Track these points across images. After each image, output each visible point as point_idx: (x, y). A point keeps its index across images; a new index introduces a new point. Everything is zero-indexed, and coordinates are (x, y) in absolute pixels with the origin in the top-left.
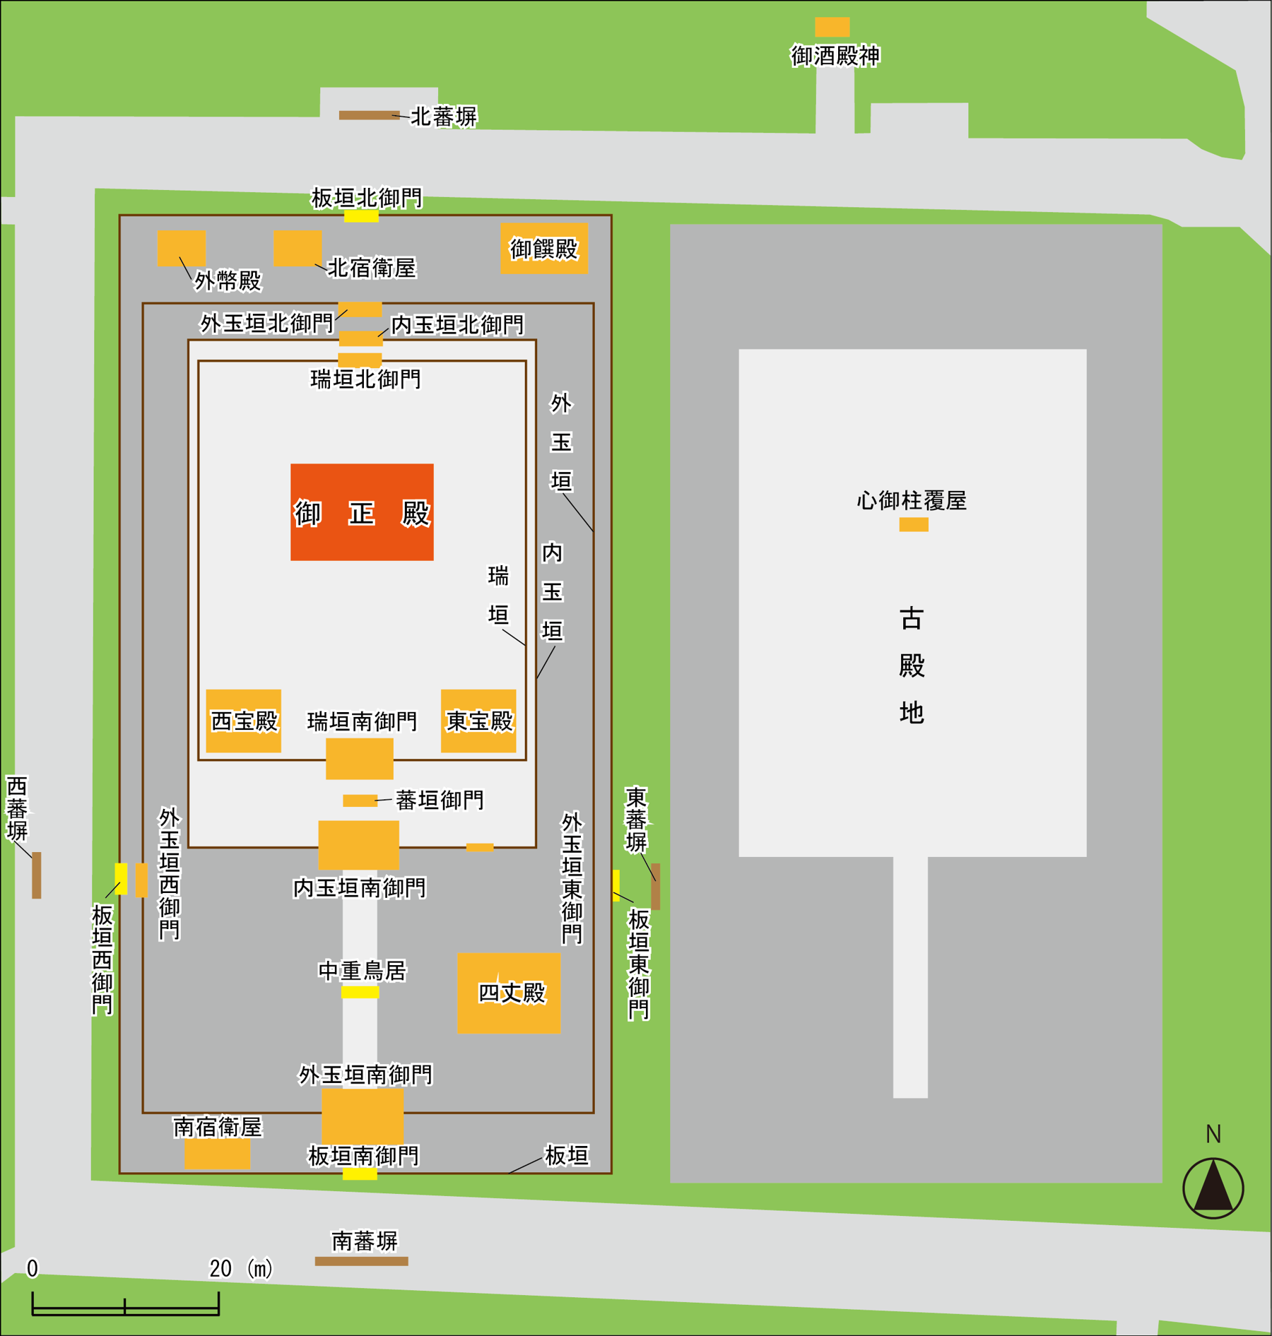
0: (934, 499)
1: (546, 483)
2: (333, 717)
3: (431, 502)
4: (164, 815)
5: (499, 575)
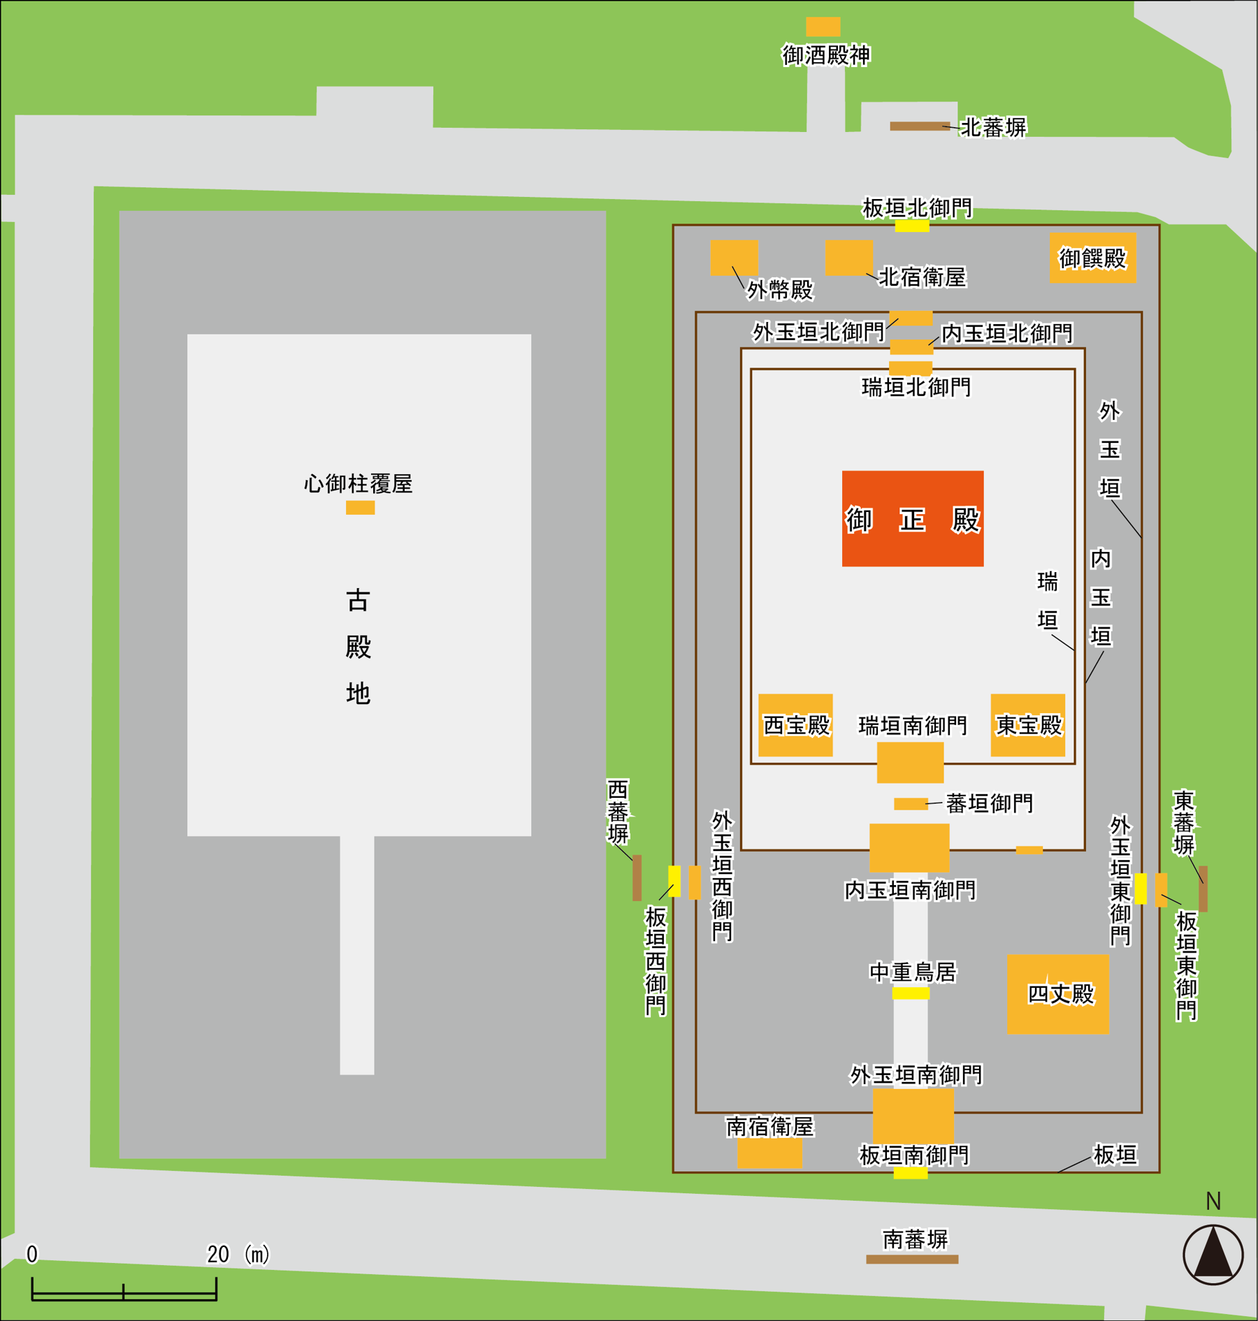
0: (381, 483)
1: (1095, 489)
2: (884, 722)
3: (981, 508)
4: (717, 818)
5: (1049, 581)
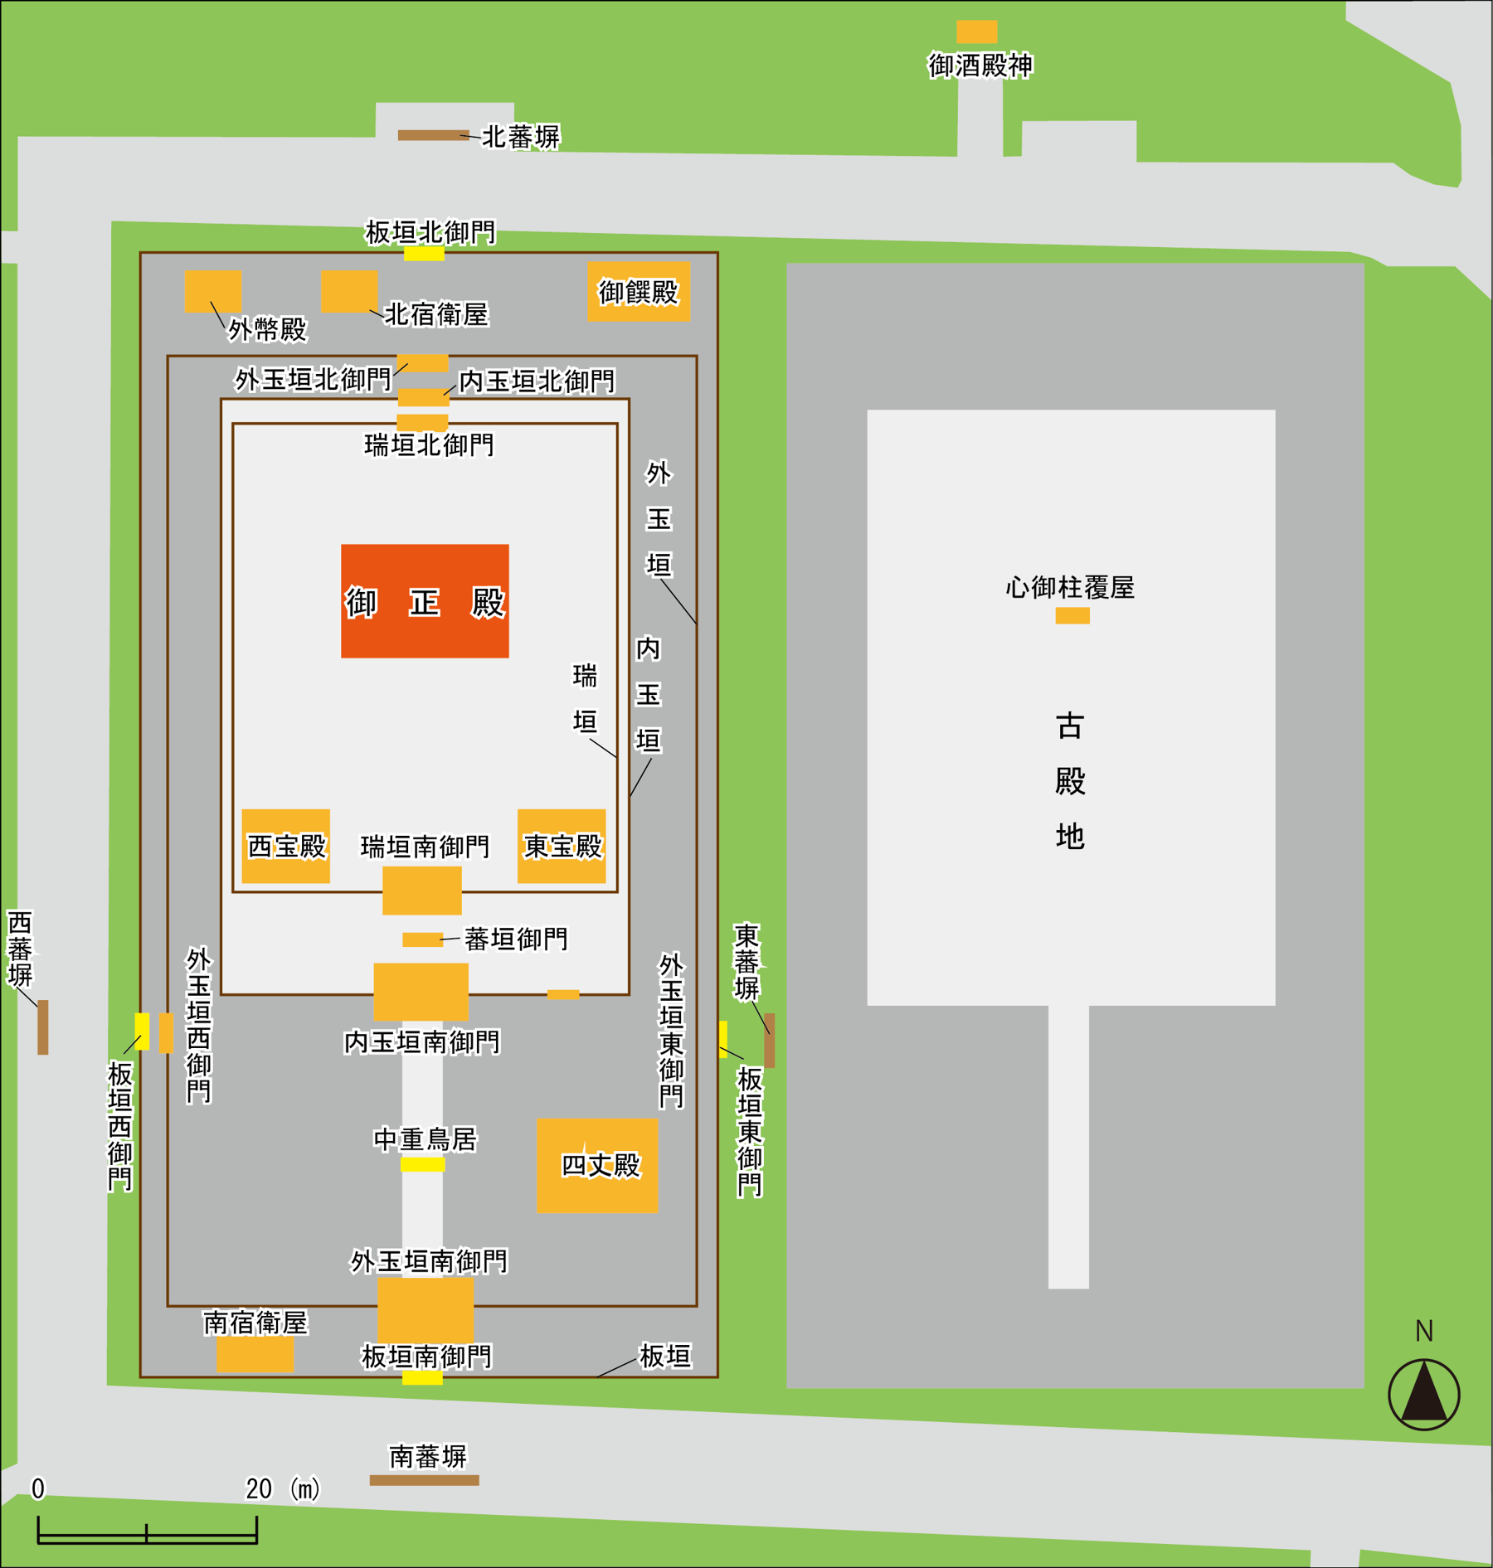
0: (1097, 586)
1: (641, 567)
2: (391, 842)
3: (506, 589)
4: (193, 957)
5: (586, 675)
